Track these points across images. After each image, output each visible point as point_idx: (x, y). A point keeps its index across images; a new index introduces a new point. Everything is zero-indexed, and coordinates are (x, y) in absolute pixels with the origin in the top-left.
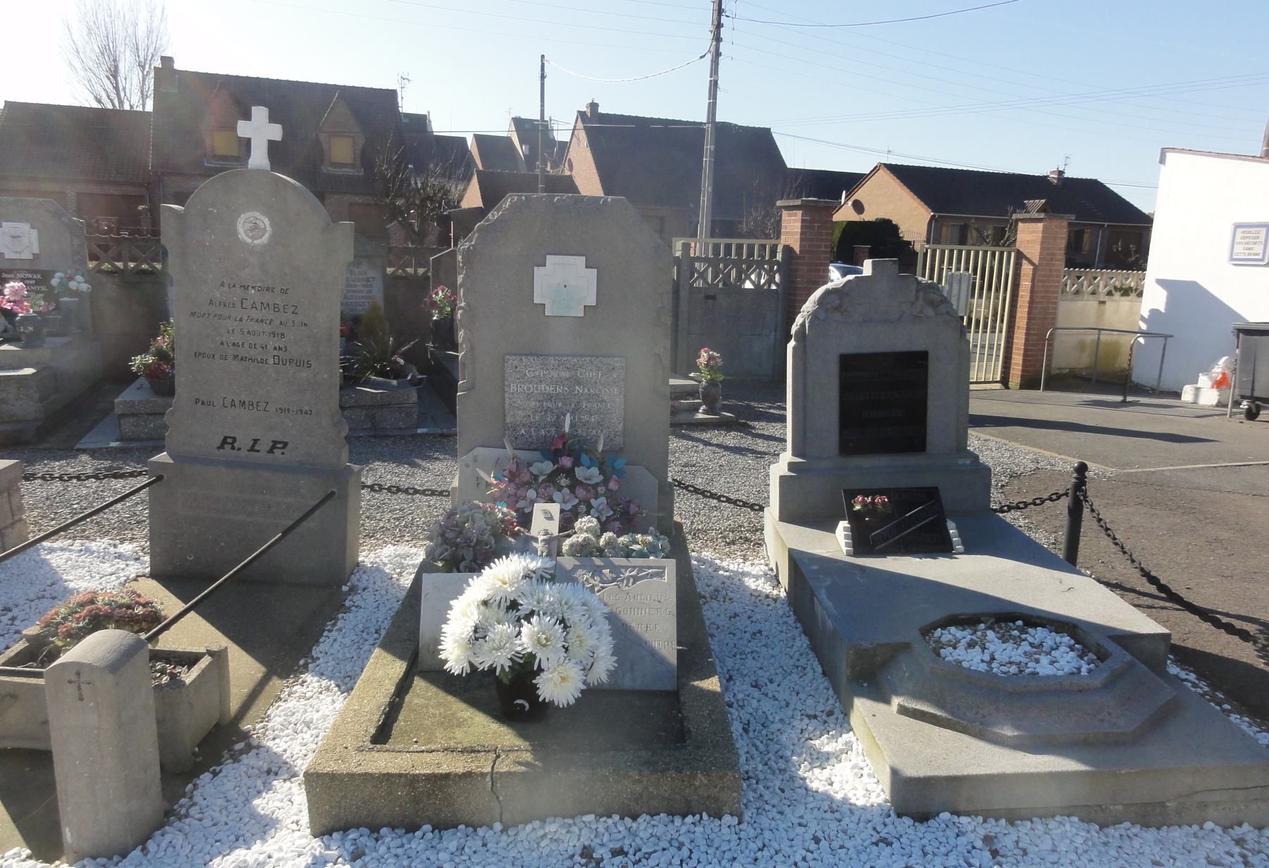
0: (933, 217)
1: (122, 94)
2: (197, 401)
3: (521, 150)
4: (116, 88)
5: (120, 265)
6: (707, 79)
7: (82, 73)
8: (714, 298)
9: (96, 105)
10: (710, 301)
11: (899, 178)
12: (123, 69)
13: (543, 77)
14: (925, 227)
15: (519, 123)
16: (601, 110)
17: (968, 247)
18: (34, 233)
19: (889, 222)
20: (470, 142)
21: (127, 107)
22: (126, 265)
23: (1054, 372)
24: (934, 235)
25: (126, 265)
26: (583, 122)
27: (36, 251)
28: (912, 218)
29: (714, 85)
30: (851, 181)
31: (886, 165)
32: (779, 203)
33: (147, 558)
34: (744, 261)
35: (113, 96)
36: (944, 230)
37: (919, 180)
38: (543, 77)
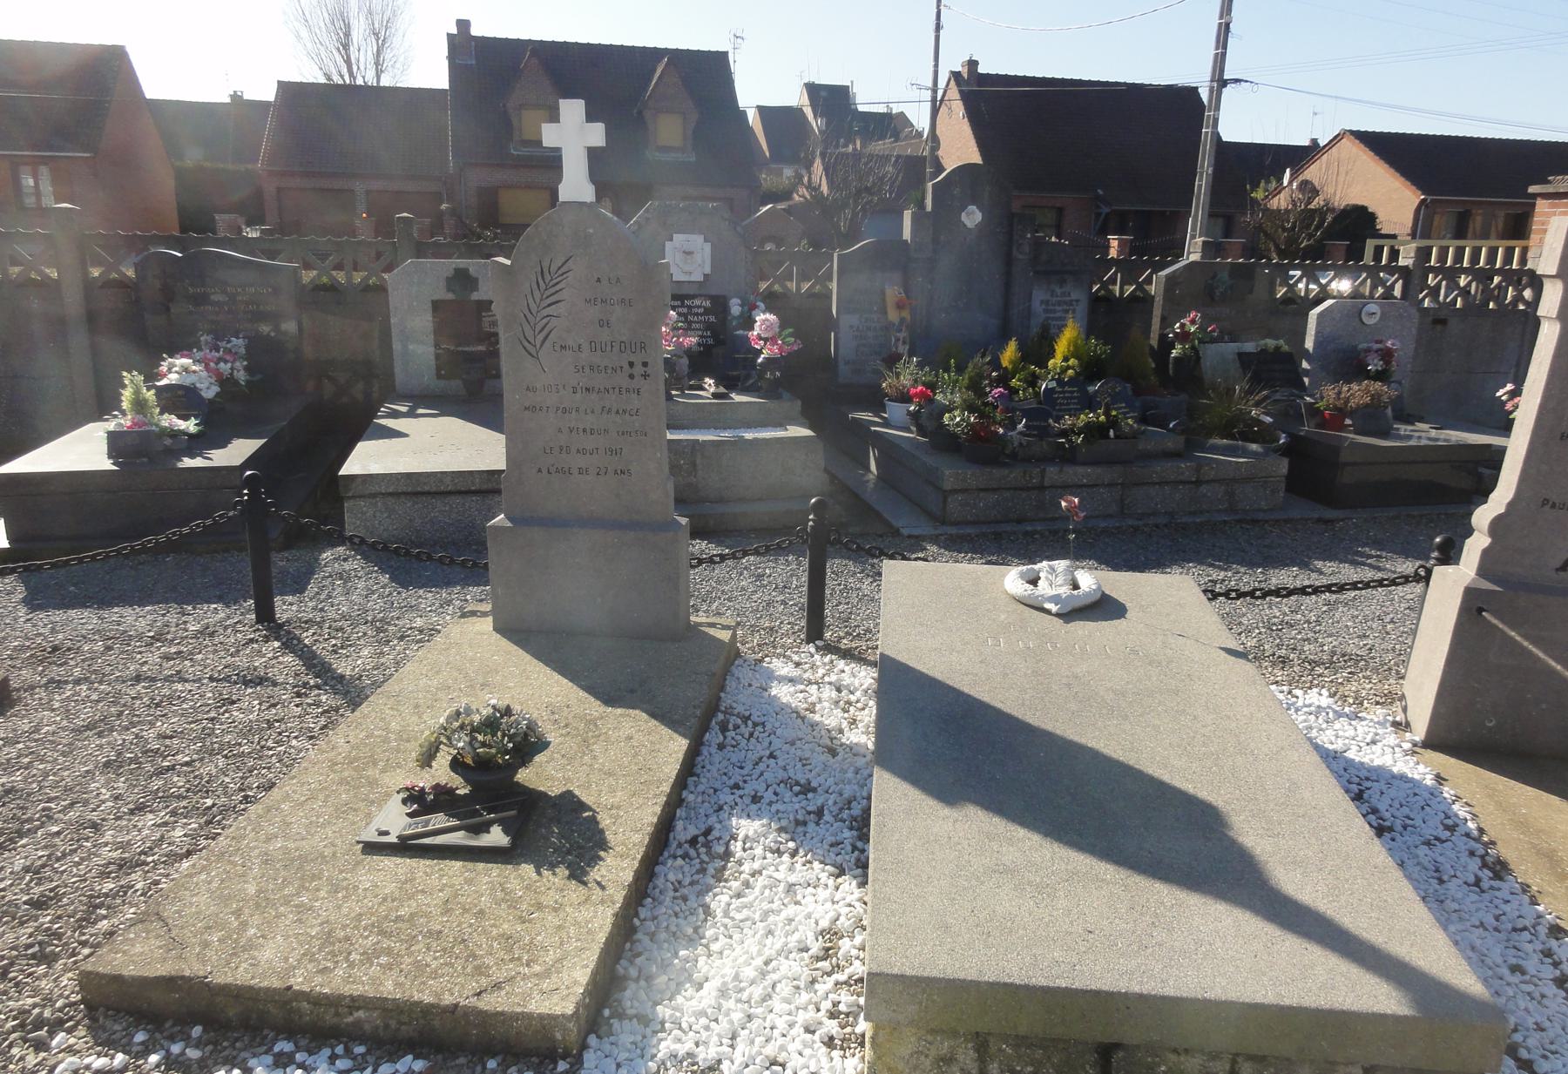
0: (1423, 201)
1: (355, 68)
2: (1545, 502)
3: (815, 123)
4: (348, 62)
5: (340, 277)
6: (1214, 21)
7: (309, 45)
8: (1443, 322)
9: (322, 80)
10: (1439, 327)
11: (1372, 149)
12: (357, 36)
13: (938, 28)
14: (1411, 216)
15: (813, 89)
16: (981, 70)
17: (1493, 243)
18: (708, 247)
19: (1363, 209)
20: (752, 116)
21: (360, 82)
22: (349, 279)
23: (456, 385)
24: (1423, 226)
25: (349, 279)
26: (958, 84)
27: (708, 270)
28: (1394, 201)
29: (1224, 31)
30: (1299, 156)
31: (1352, 133)
32: (1532, 189)
33: (872, 703)
34: (1498, 272)
35: (345, 71)
36: (1437, 218)
37: (1391, 149)
38: (938, 28)
